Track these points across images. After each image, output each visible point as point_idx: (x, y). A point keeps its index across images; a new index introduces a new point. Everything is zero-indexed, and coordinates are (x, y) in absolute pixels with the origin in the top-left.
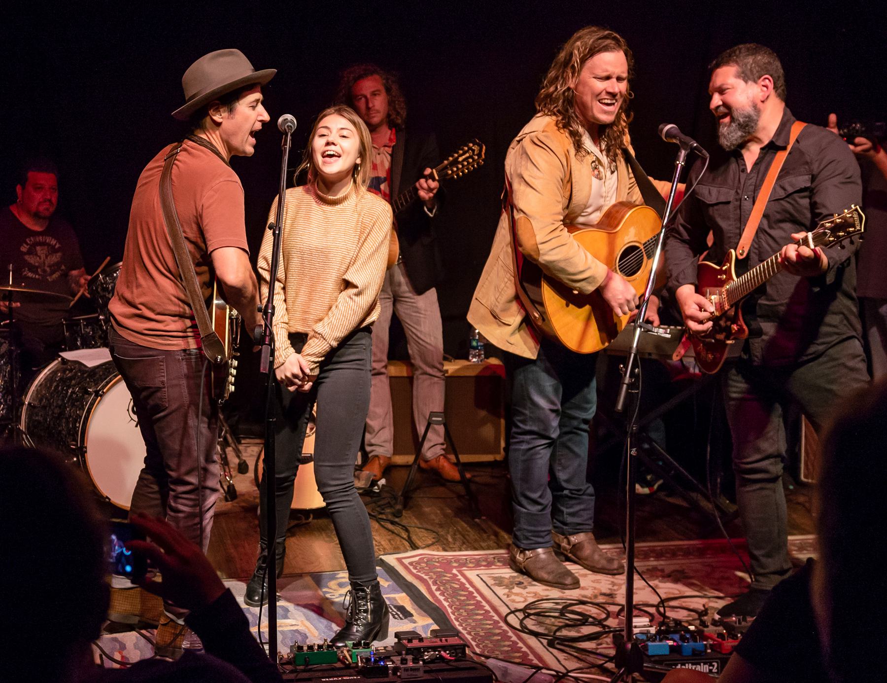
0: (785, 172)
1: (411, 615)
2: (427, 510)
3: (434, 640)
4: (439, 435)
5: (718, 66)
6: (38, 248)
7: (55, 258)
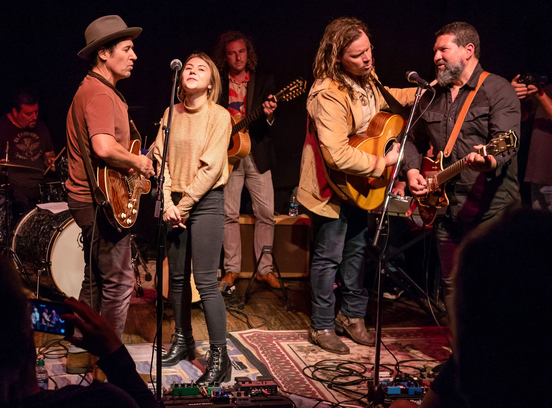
0: (474, 104)
1: (246, 368)
2: (259, 305)
3: (259, 382)
4: (269, 260)
5: (442, 33)
6: (25, 140)
7: (36, 145)
